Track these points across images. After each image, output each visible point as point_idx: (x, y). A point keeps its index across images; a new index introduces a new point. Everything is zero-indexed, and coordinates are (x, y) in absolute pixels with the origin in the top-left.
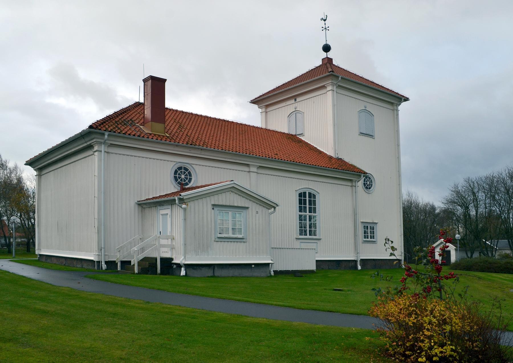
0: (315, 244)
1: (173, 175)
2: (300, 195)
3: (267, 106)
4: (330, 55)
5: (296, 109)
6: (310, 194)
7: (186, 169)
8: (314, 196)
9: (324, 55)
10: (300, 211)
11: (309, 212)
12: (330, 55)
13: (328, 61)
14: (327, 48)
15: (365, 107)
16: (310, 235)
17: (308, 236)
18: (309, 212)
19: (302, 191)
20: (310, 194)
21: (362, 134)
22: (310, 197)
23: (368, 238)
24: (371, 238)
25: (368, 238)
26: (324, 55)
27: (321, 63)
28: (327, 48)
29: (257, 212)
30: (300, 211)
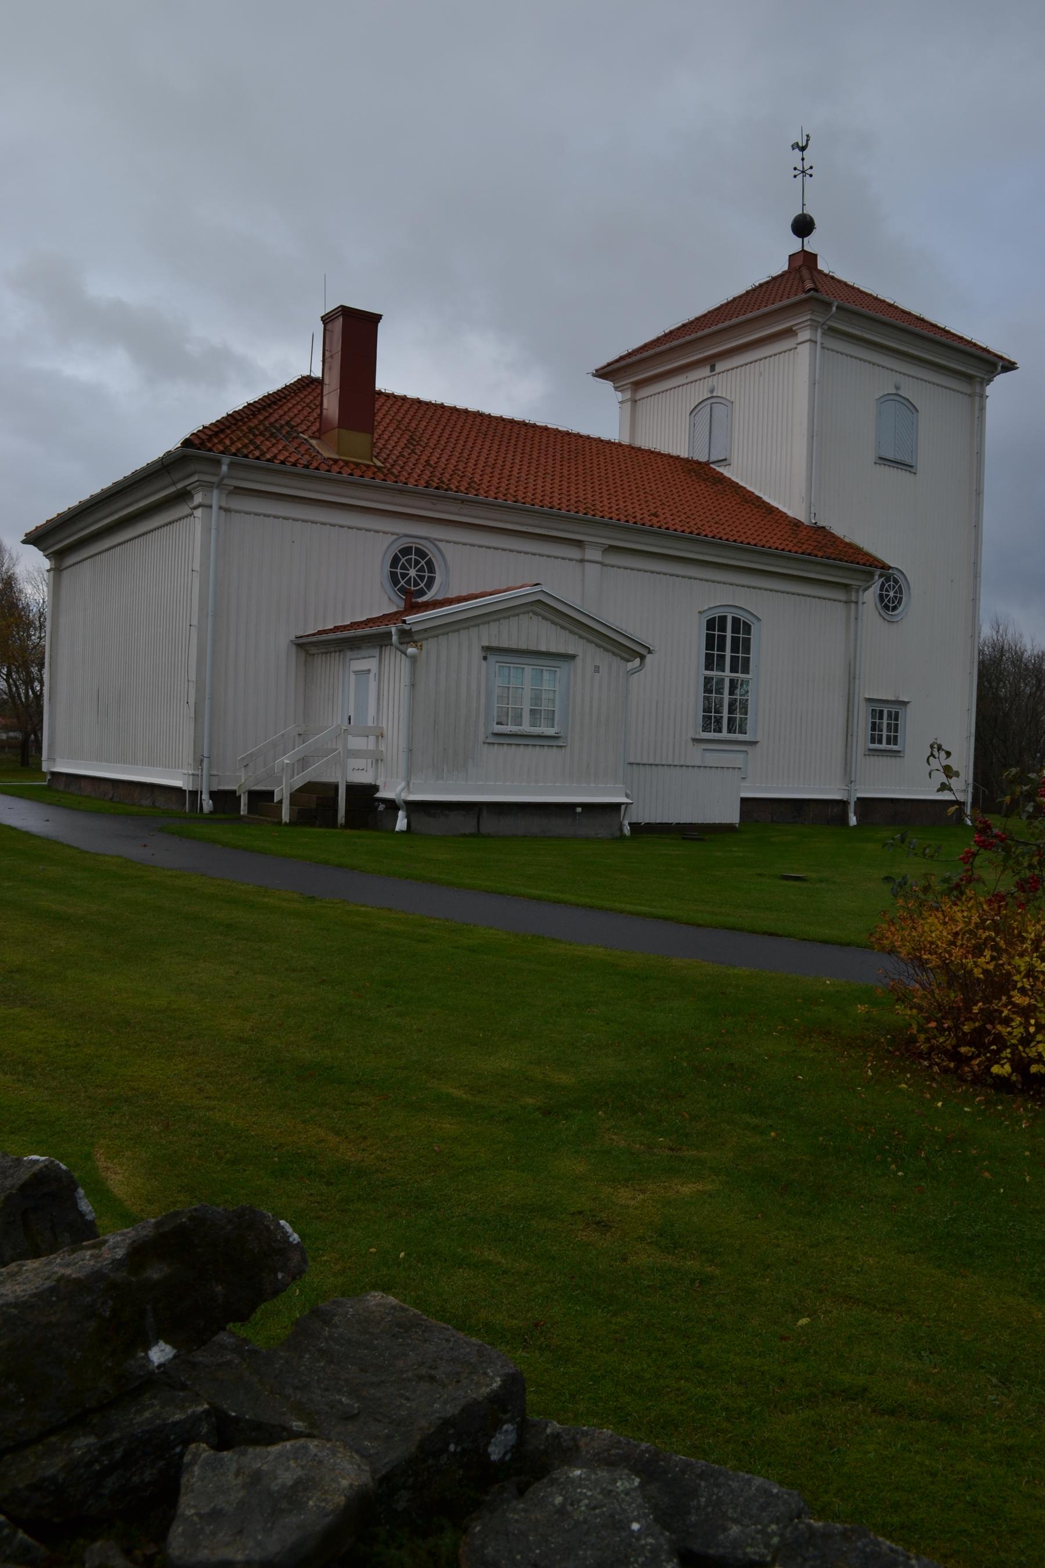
0: (742, 756)
1: (387, 568)
2: (710, 624)
3: (638, 385)
4: (812, 244)
5: (712, 391)
6: (736, 621)
7: (421, 553)
8: (748, 628)
9: (795, 244)
10: (709, 666)
11: (731, 671)
12: (812, 244)
13: (804, 262)
14: (803, 226)
15: (897, 388)
16: (729, 731)
17: (724, 735)
18: (731, 671)
19: (717, 614)
20: (736, 621)
21: (883, 460)
22: (735, 629)
23: (880, 742)
24: (888, 743)
25: (880, 742)
26: (795, 244)
27: (786, 268)
28: (803, 226)
29: (597, 669)
30: (707, 668)
